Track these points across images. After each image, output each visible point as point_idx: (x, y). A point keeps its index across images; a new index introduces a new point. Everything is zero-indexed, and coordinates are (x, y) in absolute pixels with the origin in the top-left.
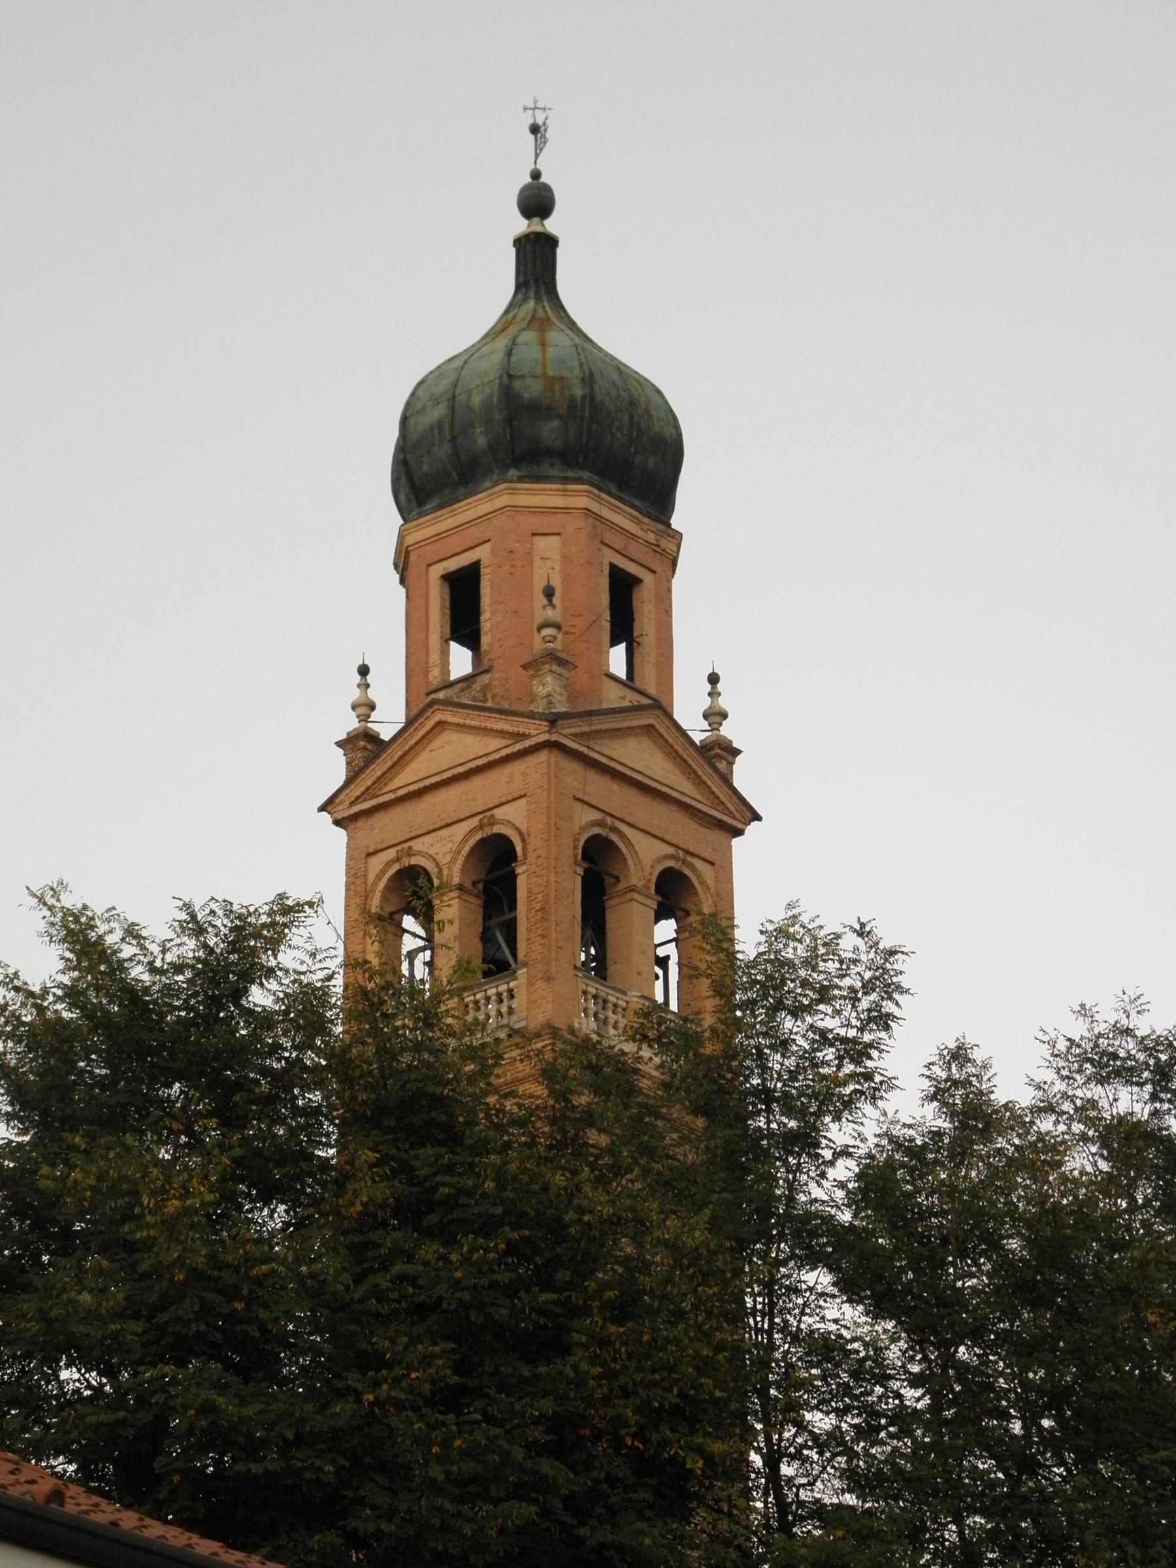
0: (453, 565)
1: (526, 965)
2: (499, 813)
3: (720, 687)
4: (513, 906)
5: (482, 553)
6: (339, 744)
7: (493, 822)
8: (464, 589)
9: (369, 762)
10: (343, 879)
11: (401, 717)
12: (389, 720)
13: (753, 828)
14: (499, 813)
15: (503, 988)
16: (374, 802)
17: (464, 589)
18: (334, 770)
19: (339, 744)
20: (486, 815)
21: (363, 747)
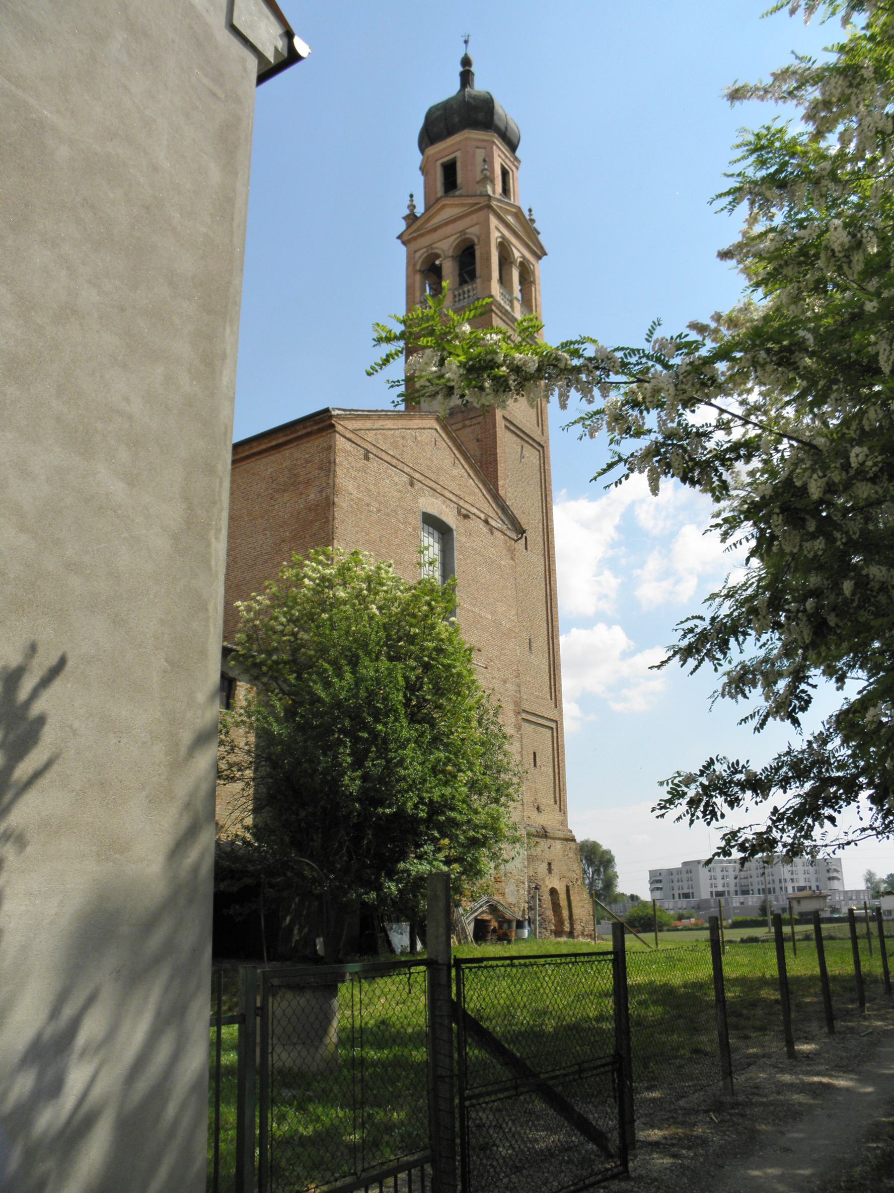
0: (445, 159)
1: (480, 277)
2: (468, 231)
3: (533, 213)
4: (474, 263)
5: (458, 154)
6: (404, 218)
7: (465, 234)
8: (450, 170)
9: (413, 223)
10: (405, 261)
11: (422, 211)
12: (420, 210)
13: (544, 258)
14: (468, 231)
15: (470, 287)
16: (295, 435)
17: (450, 170)
18: (402, 226)
19: (404, 218)
20: (463, 232)
21: (411, 218)
